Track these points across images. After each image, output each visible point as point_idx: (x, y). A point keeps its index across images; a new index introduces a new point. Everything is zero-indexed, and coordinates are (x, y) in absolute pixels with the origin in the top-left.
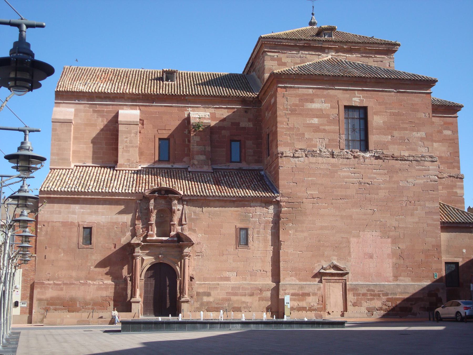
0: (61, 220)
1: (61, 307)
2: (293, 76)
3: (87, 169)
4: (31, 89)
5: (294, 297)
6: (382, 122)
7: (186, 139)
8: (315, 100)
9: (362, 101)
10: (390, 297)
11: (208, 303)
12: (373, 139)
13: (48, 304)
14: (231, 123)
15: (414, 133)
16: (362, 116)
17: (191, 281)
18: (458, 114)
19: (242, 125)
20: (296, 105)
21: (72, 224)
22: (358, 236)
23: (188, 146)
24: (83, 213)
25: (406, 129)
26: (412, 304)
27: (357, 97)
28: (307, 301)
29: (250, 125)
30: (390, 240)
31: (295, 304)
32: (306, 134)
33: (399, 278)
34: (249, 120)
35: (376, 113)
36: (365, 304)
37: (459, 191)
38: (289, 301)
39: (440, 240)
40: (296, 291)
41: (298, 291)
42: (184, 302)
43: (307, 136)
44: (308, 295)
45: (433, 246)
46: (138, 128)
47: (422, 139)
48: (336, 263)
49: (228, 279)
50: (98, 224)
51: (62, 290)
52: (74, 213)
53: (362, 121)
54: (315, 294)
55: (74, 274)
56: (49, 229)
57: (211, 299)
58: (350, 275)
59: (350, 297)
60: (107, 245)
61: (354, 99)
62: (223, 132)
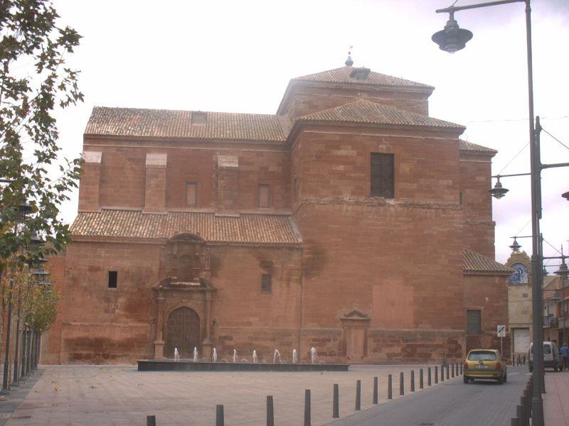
3: (135, 214)
4: (471, 38)
6: (408, 169)
17: (214, 324)
19: (271, 169)
26: (431, 351)
33: (482, 330)
36: (387, 350)
37: (489, 238)
42: (205, 345)
47: (448, 187)
49: (250, 324)
52: (100, 257)
54: (335, 340)
59: (371, 343)
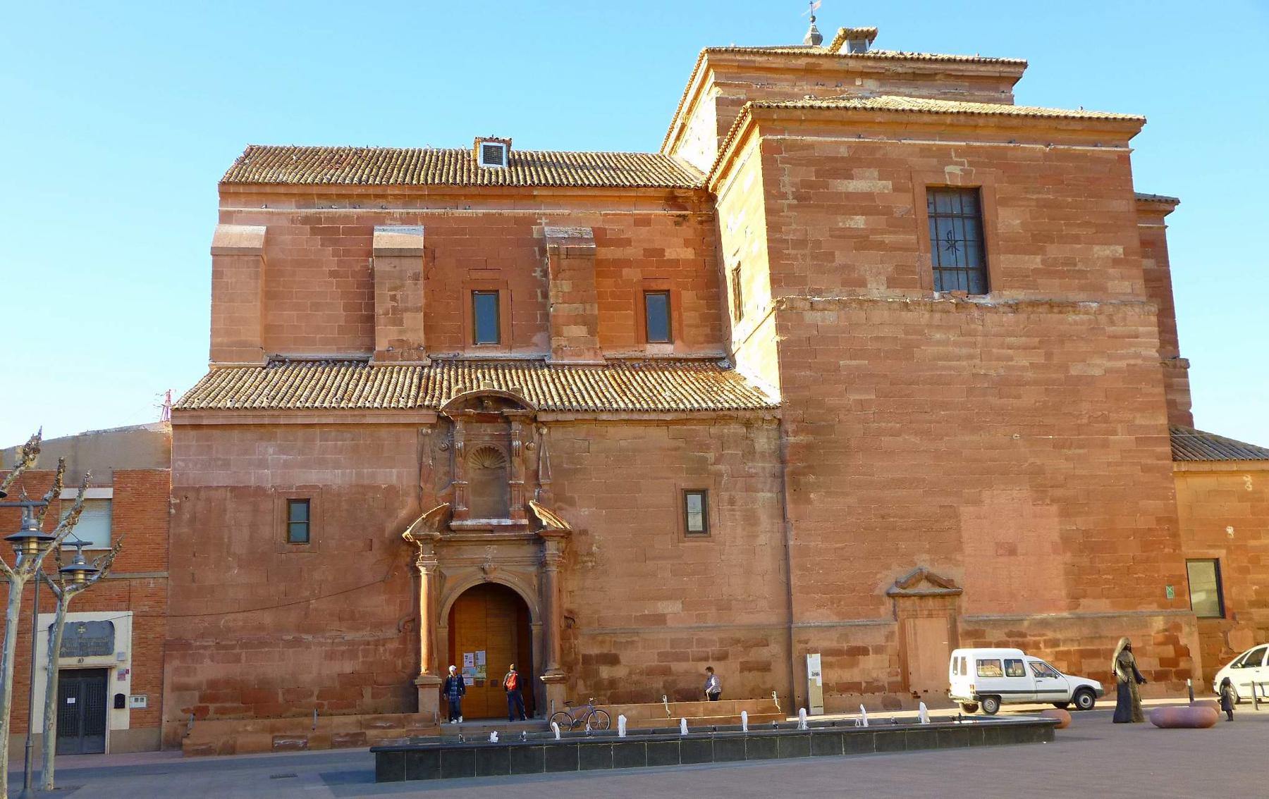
0: (230, 482)
1: (235, 705)
2: (799, 112)
5: (830, 659)
7: (539, 291)
8: (855, 171)
9: (967, 173)
10: (1061, 648)
11: (613, 683)
12: (999, 262)
13: (202, 699)
14: (645, 250)
15: (1096, 248)
16: (967, 210)
18: (1168, 219)
19: (670, 254)
20: (810, 185)
21: (259, 491)
22: (977, 502)
23: (544, 307)
24: (286, 465)
25: (1076, 239)
27: (956, 163)
28: (861, 666)
29: (689, 254)
30: (1054, 508)
31: (837, 676)
32: (837, 253)
33: (1081, 601)
34: (687, 243)
35: (1004, 202)
38: (819, 669)
39: (1175, 506)
40: (834, 645)
41: (838, 642)
43: (840, 259)
44: (864, 651)
45: (1159, 520)
46: (418, 265)
47: (1116, 262)
48: (927, 568)
50: (324, 490)
51: (237, 659)
52: (262, 464)
53: (969, 225)
54: (879, 650)
55: (267, 618)
56: (200, 506)
57: (620, 672)
58: (964, 598)
60: (349, 542)
61: (948, 169)
62: (625, 271)
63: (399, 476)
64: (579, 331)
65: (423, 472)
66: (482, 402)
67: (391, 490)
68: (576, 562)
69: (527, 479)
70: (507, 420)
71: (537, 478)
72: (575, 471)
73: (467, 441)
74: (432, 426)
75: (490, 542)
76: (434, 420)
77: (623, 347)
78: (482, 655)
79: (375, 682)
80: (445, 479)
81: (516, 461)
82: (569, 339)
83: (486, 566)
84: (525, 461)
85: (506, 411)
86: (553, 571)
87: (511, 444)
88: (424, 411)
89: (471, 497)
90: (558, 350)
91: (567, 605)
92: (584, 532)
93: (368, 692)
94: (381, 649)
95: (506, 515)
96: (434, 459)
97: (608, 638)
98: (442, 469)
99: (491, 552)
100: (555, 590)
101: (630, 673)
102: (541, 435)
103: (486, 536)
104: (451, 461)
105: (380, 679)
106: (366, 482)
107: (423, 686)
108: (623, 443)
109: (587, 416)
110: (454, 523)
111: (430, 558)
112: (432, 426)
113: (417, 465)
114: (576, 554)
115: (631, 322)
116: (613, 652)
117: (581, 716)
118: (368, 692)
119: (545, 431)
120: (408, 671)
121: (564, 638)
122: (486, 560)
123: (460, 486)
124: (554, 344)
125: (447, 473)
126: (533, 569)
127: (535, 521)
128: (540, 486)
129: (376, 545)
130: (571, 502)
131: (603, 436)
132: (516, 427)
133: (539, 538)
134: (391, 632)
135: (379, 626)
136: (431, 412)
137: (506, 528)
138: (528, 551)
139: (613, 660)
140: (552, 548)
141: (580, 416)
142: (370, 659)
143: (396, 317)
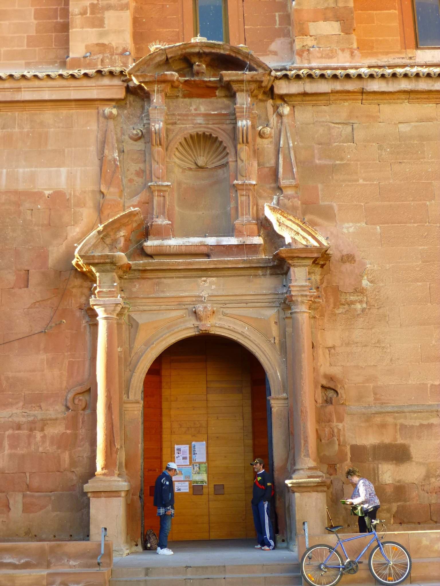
63: (70, 176)
64: (332, 28)
65: (106, 171)
66: (191, 65)
67: (59, 199)
68: (337, 304)
69: (260, 178)
70: (229, 91)
71: (276, 178)
72: (334, 169)
73: (170, 123)
74: (118, 102)
75: (205, 271)
76: (121, 94)
77: (387, 53)
78: (201, 447)
79: (29, 487)
80: (139, 181)
81: (244, 151)
82: (316, 38)
83: (200, 308)
84: (256, 153)
85: (229, 75)
86: (303, 313)
87: (235, 128)
88: (106, 81)
89: (177, 208)
90: (304, 51)
91: (325, 368)
92: (349, 258)
93: (17, 502)
94: (38, 435)
95: (230, 232)
96: (121, 152)
97: (390, 420)
98: (134, 167)
99: (207, 287)
100: (306, 344)
101: (428, 477)
102: (280, 116)
103: (199, 264)
104: (145, 156)
105: (36, 482)
106: (22, 187)
107: (97, 494)
108: (404, 128)
109: (350, 86)
110: (151, 243)
111: (110, 294)
112: (118, 102)
113: (96, 162)
114: (336, 290)
115: (395, 24)
116: (400, 441)
117: (357, 552)
118: (17, 502)
119: (286, 110)
120: (79, 470)
121: (322, 419)
122: (199, 299)
123: (161, 190)
124: (297, 46)
125: (140, 173)
126: (271, 314)
127: (273, 238)
128: (280, 189)
129: (35, 279)
130: (327, 214)
131: (374, 118)
132: (243, 100)
133: (279, 266)
134: (55, 410)
135: (36, 400)
136: (116, 82)
137: (228, 249)
138: (265, 284)
139: (399, 455)
140: (300, 276)
141: (338, 86)
142: (20, 451)
143: (96, 16)
